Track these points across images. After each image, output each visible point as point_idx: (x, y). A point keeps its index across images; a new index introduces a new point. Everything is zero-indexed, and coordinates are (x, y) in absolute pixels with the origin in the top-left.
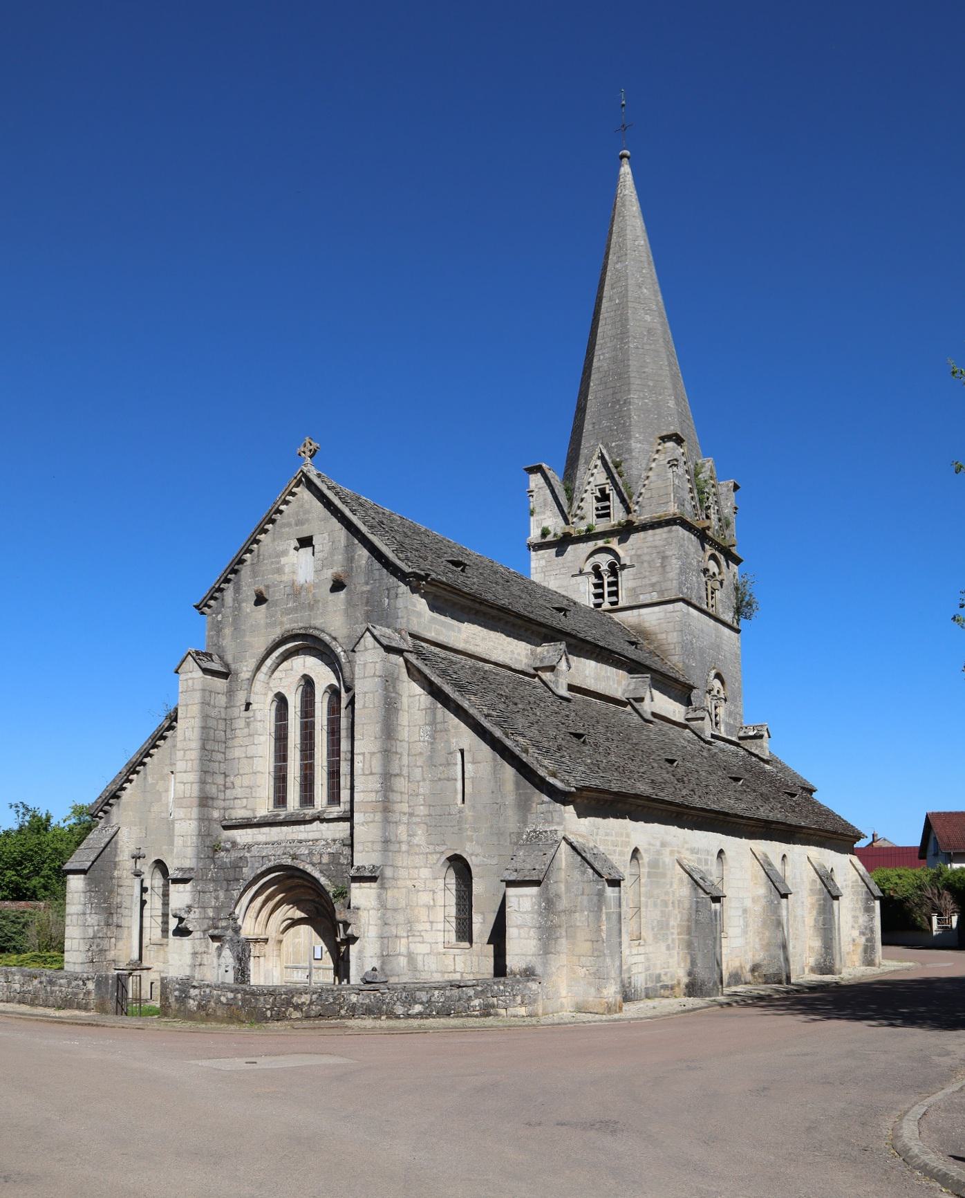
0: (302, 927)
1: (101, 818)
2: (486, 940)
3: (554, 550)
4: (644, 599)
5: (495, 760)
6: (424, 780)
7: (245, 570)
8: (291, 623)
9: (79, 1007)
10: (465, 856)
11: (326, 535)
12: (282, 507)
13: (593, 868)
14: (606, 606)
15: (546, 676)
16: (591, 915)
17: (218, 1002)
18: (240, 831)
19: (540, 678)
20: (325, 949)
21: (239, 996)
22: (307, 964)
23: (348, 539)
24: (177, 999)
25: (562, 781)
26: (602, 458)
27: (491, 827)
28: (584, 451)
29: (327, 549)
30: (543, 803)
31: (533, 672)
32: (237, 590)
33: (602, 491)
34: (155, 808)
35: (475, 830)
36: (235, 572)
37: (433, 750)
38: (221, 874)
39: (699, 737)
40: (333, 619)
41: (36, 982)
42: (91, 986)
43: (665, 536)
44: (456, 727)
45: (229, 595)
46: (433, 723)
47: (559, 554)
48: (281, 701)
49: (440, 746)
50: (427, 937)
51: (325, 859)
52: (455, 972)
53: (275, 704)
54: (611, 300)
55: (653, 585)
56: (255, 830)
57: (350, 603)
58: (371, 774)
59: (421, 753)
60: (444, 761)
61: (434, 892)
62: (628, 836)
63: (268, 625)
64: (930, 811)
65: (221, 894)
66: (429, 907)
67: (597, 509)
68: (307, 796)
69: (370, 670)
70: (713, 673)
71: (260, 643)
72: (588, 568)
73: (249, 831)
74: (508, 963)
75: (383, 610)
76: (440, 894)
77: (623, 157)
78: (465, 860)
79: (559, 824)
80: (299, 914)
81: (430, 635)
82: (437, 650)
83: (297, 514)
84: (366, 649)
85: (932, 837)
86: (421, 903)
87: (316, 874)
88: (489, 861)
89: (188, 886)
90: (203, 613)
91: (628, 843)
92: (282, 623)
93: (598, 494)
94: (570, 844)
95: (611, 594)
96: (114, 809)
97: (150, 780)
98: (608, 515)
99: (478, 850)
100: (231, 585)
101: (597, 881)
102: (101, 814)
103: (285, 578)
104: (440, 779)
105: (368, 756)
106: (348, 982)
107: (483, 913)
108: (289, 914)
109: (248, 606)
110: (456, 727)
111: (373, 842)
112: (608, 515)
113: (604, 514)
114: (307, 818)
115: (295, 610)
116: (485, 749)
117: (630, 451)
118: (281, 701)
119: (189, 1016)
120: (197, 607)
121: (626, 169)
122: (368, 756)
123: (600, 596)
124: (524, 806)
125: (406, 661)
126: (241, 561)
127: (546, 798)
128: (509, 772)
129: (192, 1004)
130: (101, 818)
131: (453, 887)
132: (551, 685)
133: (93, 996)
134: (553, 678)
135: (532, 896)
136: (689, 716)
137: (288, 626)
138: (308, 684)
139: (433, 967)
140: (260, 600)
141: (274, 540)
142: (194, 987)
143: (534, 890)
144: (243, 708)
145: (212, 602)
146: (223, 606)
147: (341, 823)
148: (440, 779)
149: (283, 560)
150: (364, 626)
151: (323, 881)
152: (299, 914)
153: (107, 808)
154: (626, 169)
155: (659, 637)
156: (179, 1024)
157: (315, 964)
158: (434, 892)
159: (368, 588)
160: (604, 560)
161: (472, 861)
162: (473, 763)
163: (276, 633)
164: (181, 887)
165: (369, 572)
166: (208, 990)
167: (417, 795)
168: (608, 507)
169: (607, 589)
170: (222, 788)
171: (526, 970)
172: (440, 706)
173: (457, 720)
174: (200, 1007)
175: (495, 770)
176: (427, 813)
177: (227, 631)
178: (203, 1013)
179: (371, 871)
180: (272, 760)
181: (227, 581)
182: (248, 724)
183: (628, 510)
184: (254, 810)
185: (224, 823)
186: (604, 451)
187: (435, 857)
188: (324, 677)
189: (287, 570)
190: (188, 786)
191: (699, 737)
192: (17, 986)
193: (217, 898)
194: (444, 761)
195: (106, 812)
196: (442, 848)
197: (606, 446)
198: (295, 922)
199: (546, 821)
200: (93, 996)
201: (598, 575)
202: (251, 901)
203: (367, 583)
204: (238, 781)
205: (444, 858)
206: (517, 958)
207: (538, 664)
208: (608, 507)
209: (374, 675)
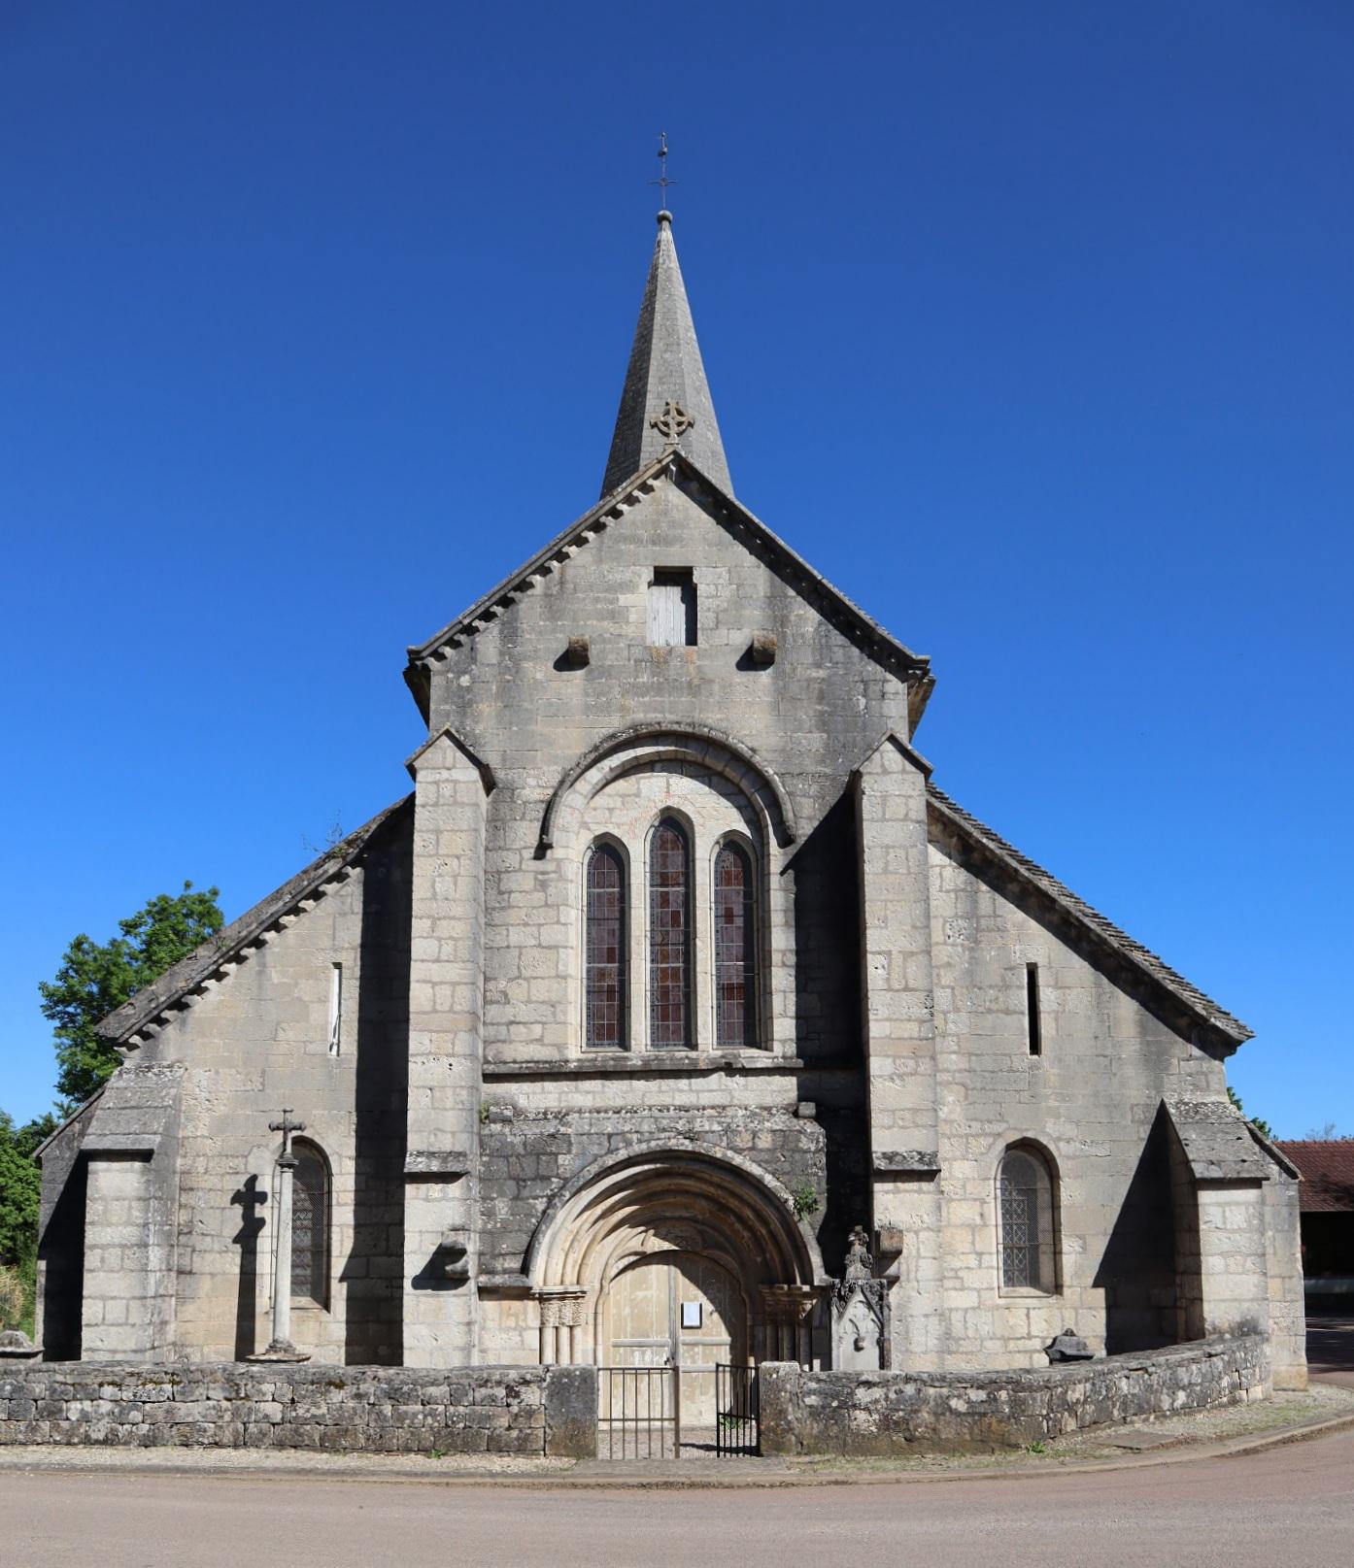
0: (654, 1268)
1: (133, 1047)
2: (1091, 1281)
5: (1098, 985)
6: (957, 1010)
7: (529, 605)
9: (495, 1446)
10: (1044, 1140)
11: (723, 571)
12: (624, 507)
16: (1279, 1236)
17: (943, 1409)
18: (526, 1086)
20: (709, 1307)
21: (1003, 1395)
22: (666, 1338)
23: (772, 584)
24: (814, 1412)
27: (1096, 1094)
29: (727, 592)
30: (1191, 1058)
32: (510, 635)
34: (290, 1034)
35: (1063, 1098)
36: (506, 602)
37: (974, 961)
38: (500, 1166)
41: (337, 1396)
42: (534, 1396)
44: (1021, 926)
45: (489, 641)
46: (972, 915)
48: (609, 854)
49: (989, 954)
50: (970, 1279)
51: (765, 1142)
52: (1029, 1337)
53: (589, 853)
54: (659, 396)
57: (782, 694)
58: (906, 989)
59: (949, 964)
60: (997, 980)
63: (588, 709)
65: (502, 1207)
66: (974, 1229)
69: (896, 808)
71: (574, 742)
73: (549, 1085)
74: (1206, 1315)
75: (857, 715)
77: (664, 218)
80: (656, 1244)
83: (655, 524)
84: (885, 772)
86: (954, 1220)
87: (755, 1170)
88: (1094, 1151)
89: (455, 1189)
92: (623, 709)
96: (170, 1029)
97: (275, 977)
99: (1070, 1131)
100: (494, 627)
101: (1286, 1185)
102: (136, 1039)
103: (630, 631)
104: (990, 1011)
106: (827, 1365)
107: (1082, 1237)
108: (635, 1244)
109: (540, 670)
110: (1021, 926)
111: (915, 1111)
114: (702, 1066)
115: (658, 689)
116: (1078, 968)
119: (857, 1446)
121: (666, 235)
124: (1155, 1062)
126: (524, 586)
127: (1196, 1052)
128: (1126, 1007)
129: (863, 1421)
130: (133, 1047)
133: (540, 1421)
135: (1247, 1204)
137: (640, 717)
138: (674, 828)
139: (985, 1330)
140: (573, 659)
141: (600, 561)
142: (869, 1384)
143: (1250, 1195)
144: (530, 853)
145: (448, 651)
146: (474, 660)
147: (777, 1079)
148: (990, 1011)
149: (624, 599)
151: (769, 1180)
152: (656, 1244)
153: (153, 1027)
154: (666, 235)
156: (843, 1467)
157: (684, 1336)
158: (983, 1202)
159: (822, 673)
161: (1060, 1151)
162: (1057, 987)
163: (614, 724)
164: (435, 1190)
165: (823, 650)
166: (910, 1389)
171: (1241, 1325)
172: (984, 887)
173: (1021, 915)
174: (886, 1424)
175: (1099, 1002)
176: (964, 1065)
177: (487, 708)
178: (898, 1438)
181: (487, 616)
182: (543, 886)
184: (561, 1047)
185: (490, 1069)
187: (985, 1142)
188: (714, 817)
189: (633, 617)
190: (445, 991)
192: (274, 1410)
193: (489, 1214)
194: (997, 980)
195: (146, 1036)
198: (645, 1259)
199: (1196, 1087)
200: (540, 1421)
202: (603, 1216)
203: (818, 666)
204: (517, 992)
205: (1001, 1145)
206: (1223, 1306)
209: (906, 818)
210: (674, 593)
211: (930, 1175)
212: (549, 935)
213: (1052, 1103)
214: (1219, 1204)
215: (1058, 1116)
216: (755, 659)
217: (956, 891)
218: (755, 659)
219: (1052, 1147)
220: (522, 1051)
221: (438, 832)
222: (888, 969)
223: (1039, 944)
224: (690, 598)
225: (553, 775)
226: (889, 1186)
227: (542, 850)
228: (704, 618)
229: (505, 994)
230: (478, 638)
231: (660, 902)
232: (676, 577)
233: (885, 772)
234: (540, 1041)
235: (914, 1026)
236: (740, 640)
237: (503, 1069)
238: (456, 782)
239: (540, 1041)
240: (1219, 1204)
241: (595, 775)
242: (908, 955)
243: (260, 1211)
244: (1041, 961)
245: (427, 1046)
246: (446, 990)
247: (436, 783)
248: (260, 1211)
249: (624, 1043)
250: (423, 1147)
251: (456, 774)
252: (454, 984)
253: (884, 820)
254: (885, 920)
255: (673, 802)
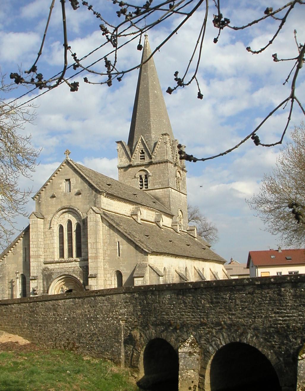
3: (124, 169)
4: (156, 187)
6: (107, 250)
8: (65, 204)
10: (120, 270)
13: (156, 273)
14: (144, 189)
15: (135, 217)
18: (50, 265)
19: (133, 218)
25: (147, 250)
26: (142, 140)
28: (135, 137)
31: (131, 216)
33: (142, 151)
39: (176, 232)
40: (79, 204)
43: (164, 166)
47: (125, 171)
48: (61, 228)
55: (160, 182)
56: (55, 264)
58: (94, 248)
61: (111, 281)
62: (163, 264)
64: (250, 251)
67: (141, 156)
68: (70, 255)
70: (179, 210)
71: (54, 210)
72: (138, 175)
76: (113, 281)
78: (120, 272)
79: (147, 261)
81: (106, 208)
82: (107, 212)
85: (251, 260)
90: (34, 200)
91: (163, 266)
93: (141, 152)
94: (151, 267)
95: (145, 185)
98: (144, 159)
100: (43, 192)
105: (92, 244)
112: (144, 159)
113: (143, 158)
116: (125, 242)
117: (151, 137)
118: (61, 228)
120: (32, 198)
122: (92, 244)
123: (142, 185)
125: (101, 216)
131: (116, 279)
132: (137, 220)
134: (136, 218)
136: (173, 225)
140: (53, 197)
150: (88, 206)
155: (162, 199)
160: (143, 174)
161: (122, 272)
164: (34, 281)
167: (106, 254)
168: (144, 156)
169: (144, 183)
170: (43, 252)
179: (94, 275)
180: (59, 244)
182: (51, 234)
183: (151, 158)
184: (54, 259)
185: (45, 263)
186: (143, 138)
191: (176, 232)
196: (114, 269)
197: (143, 136)
201: (141, 178)
207: (132, 214)
208: (144, 156)
210: (68, 182)
211: (95, 277)
212: (52, 241)
213: (121, 264)
214: (137, 281)
215: (122, 266)
216: (78, 194)
217: (107, 230)
218: (78, 194)
219: (121, 272)
220: (49, 260)
221: (33, 228)
222: (91, 245)
223: (120, 239)
224: (70, 183)
225: (52, 216)
226: (91, 279)
227: (50, 228)
228: (72, 187)
229: (46, 251)
230: (41, 194)
231: (68, 234)
232: (68, 180)
233: (91, 213)
234: (51, 258)
235: (94, 254)
236: (76, 190)
237: (46, 263)
238: (35, 220)
239: (51, 258)
240: (137, 281)
241: (64, 210)
242: (94, 243)
243: (14, 284)
244: (120, 241)
245: (33, 261)
246: (34, 252)
247: (32, 221)
248: (14, 284)
249: (63, 258)
250: (32, 275)
251: (35, 219)
252: (36, 251)
253: (91, 221)
254: (90, 238)
255: (69, 219)
